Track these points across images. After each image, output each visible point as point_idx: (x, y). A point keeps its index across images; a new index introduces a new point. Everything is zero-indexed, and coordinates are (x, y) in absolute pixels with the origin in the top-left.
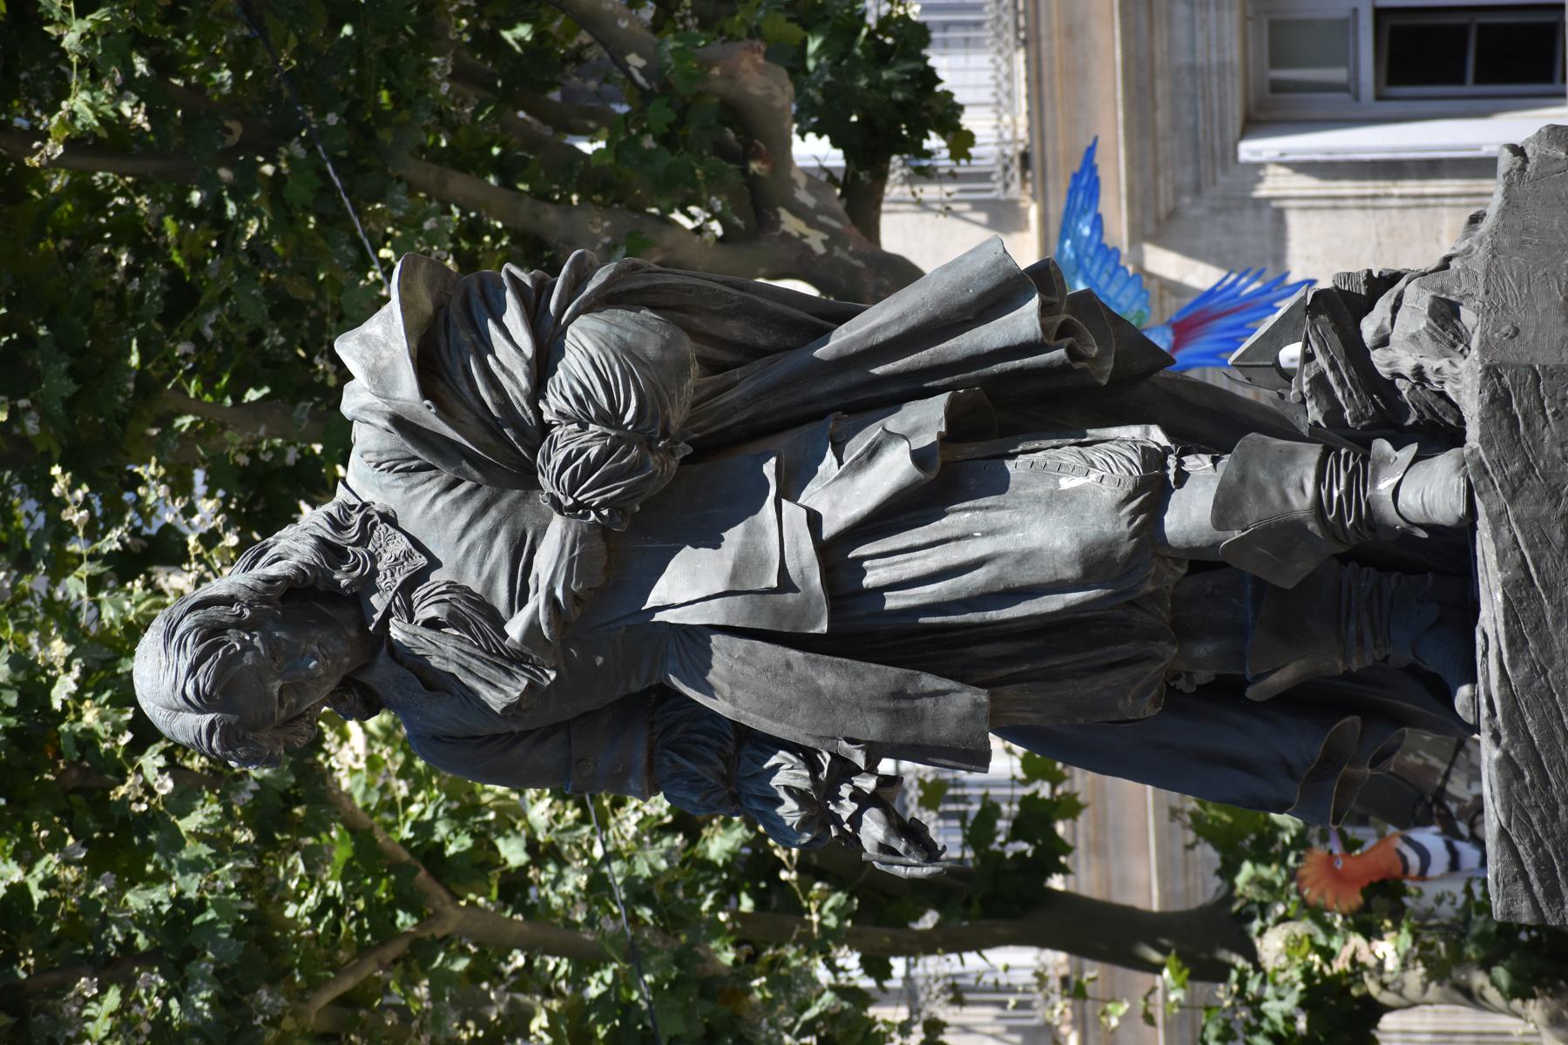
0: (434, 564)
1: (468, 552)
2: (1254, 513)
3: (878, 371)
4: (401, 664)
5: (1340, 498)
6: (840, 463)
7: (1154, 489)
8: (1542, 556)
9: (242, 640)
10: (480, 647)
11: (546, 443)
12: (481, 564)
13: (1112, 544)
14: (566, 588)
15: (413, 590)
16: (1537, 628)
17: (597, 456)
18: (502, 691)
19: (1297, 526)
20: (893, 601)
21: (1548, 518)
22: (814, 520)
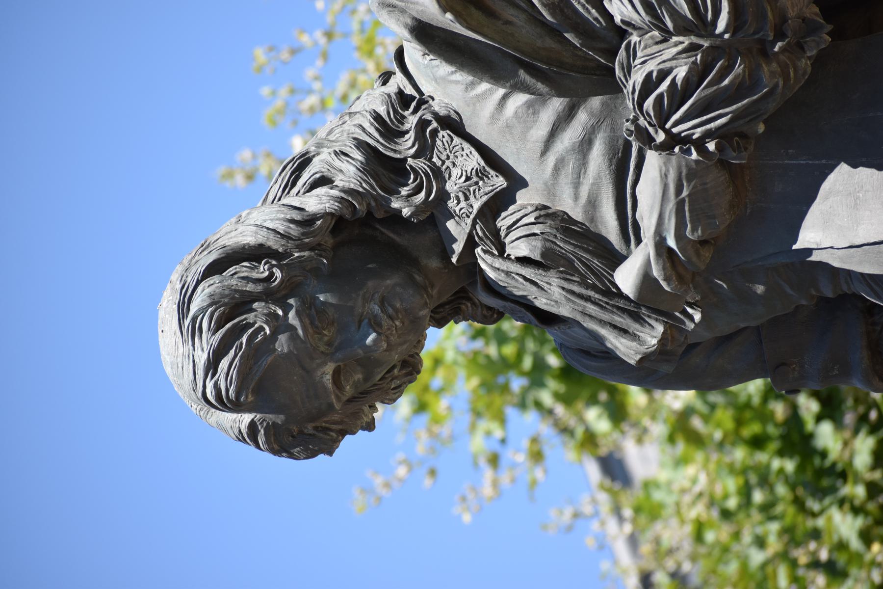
0: (516, 182)
1: (557, 169)
9: (273, 316)
11: (622, 53)
12: (577, 185)
14: (679, 236)
15: (496, 215)
17: (686, 79)
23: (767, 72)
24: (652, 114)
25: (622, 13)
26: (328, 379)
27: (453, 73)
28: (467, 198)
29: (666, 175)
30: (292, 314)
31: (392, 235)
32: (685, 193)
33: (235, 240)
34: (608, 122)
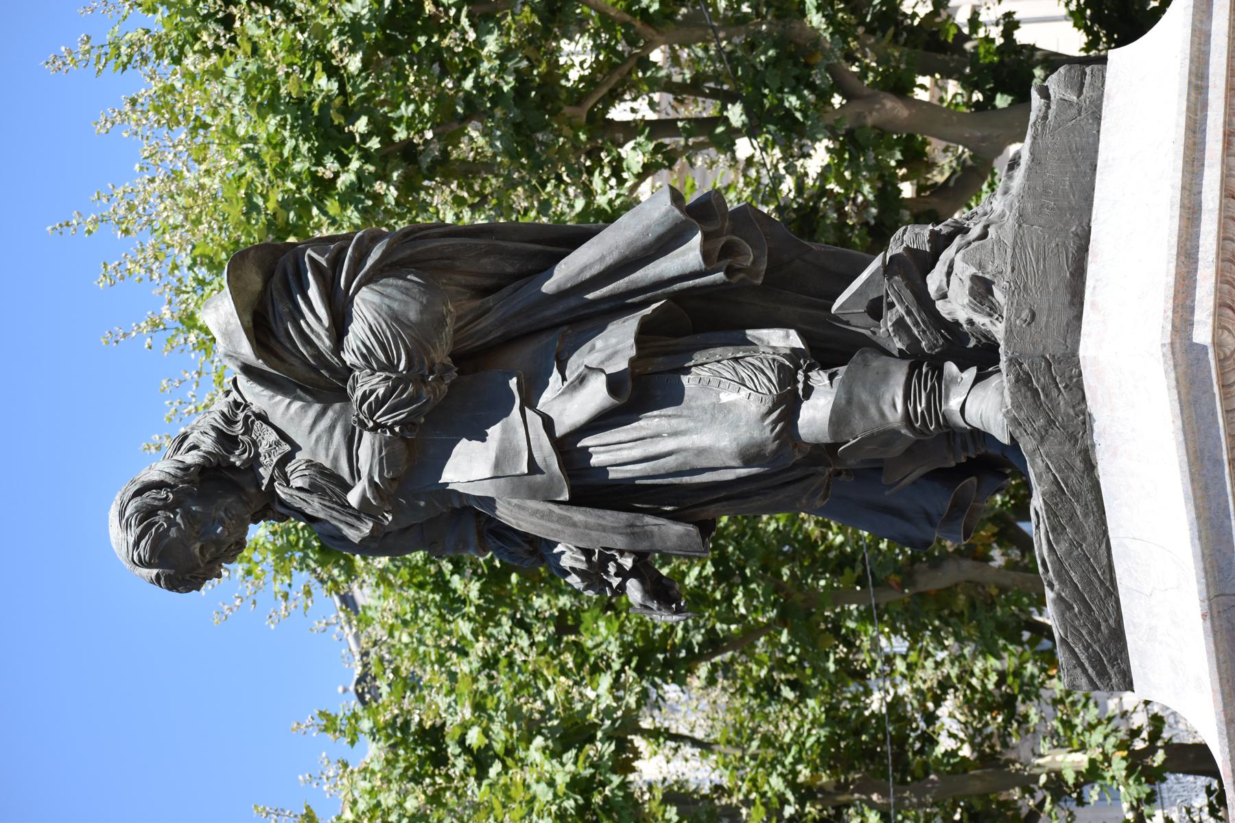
1: (317, 441)
2: (860, 428)
3: (590, 296)
5: (922, 412)
6: (564, 379)
7: (788, 403)
8: (1068, 477)
11: (351, 380)
12: (327, 449)
13: (761, 445)
14: (381, 476)
16: (1071, 519)
17: (384, 394)
19: (895, 433)
20: (614, 474)
21: (1069, 454)
22: (548, 424)
26: (197, 551)
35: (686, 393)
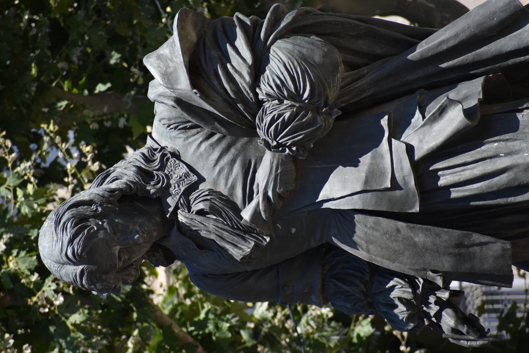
0: (201, 179)
1: (220, 172)
3: (444, 65)
4: (185, 235)
6: (424, 117)
10: (228, 225)
11: (261, 111)
12: (227, 179)
14: (274, 191)
18: (241, 249)
20: (455, 193)
22: (410, 149)
23: (320, 119)
24: (272, 134)
25: (266, 91)
26: (117, 252)
27: (179, 134)
28: (179, 186)
29: (273, 163)
30: (105, 224)
31: (141, 206)
32: (279, 171)
33: (79, 199)
34: (243, 153)
35: (521, 123)
